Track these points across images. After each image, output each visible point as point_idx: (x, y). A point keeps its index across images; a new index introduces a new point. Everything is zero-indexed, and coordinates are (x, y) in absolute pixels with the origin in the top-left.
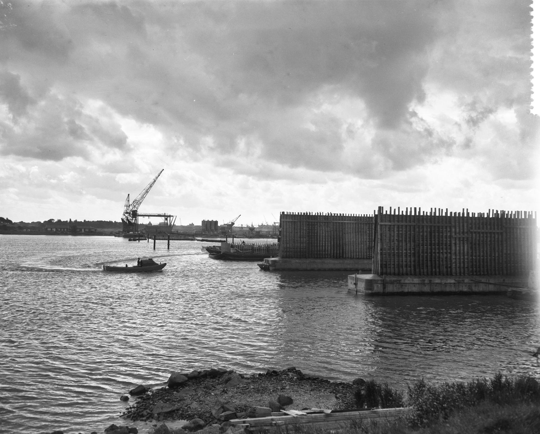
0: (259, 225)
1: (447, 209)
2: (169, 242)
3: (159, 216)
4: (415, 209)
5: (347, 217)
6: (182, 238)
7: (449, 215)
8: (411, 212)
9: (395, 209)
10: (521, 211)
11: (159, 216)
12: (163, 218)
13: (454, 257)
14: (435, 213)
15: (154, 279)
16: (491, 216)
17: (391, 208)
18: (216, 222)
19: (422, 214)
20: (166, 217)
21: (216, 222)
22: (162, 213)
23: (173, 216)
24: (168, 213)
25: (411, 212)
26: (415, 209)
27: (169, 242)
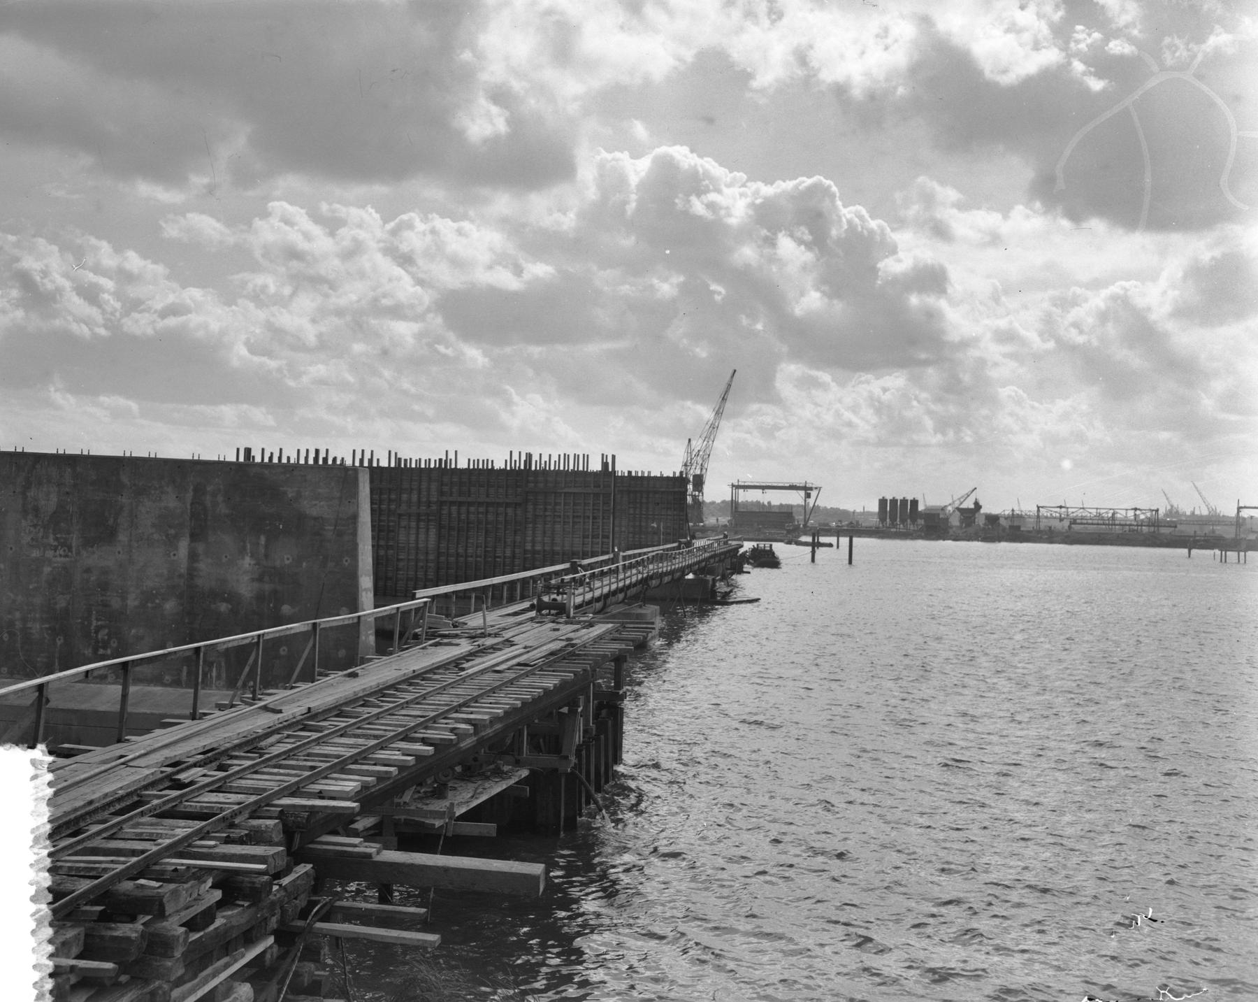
0: (769, 503)
1: (327, 450)
2: (813, 553)
3: (792, 487)
4: (317, 451)
5: (284, 466)
6: (751, 537)
7: (330, 462)
8: (306, 458)
9: (272, 454)
10: (411, 459)
11: (792, 487)
12: (802, 493)
13: (452, 559)
14: (271, 458)
15: (357, 679)
16: (432, 466)
17: (263, 450)
18: (915, 503)
19: (284, 460)
20: (807, 490)
21: (915, 503)
22: (798, 481)
23: (819, 489)
24: (811, 482)
25: (306, 458)
26: (317, 451)
27: (813, 553)
